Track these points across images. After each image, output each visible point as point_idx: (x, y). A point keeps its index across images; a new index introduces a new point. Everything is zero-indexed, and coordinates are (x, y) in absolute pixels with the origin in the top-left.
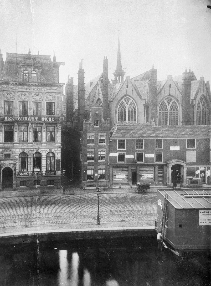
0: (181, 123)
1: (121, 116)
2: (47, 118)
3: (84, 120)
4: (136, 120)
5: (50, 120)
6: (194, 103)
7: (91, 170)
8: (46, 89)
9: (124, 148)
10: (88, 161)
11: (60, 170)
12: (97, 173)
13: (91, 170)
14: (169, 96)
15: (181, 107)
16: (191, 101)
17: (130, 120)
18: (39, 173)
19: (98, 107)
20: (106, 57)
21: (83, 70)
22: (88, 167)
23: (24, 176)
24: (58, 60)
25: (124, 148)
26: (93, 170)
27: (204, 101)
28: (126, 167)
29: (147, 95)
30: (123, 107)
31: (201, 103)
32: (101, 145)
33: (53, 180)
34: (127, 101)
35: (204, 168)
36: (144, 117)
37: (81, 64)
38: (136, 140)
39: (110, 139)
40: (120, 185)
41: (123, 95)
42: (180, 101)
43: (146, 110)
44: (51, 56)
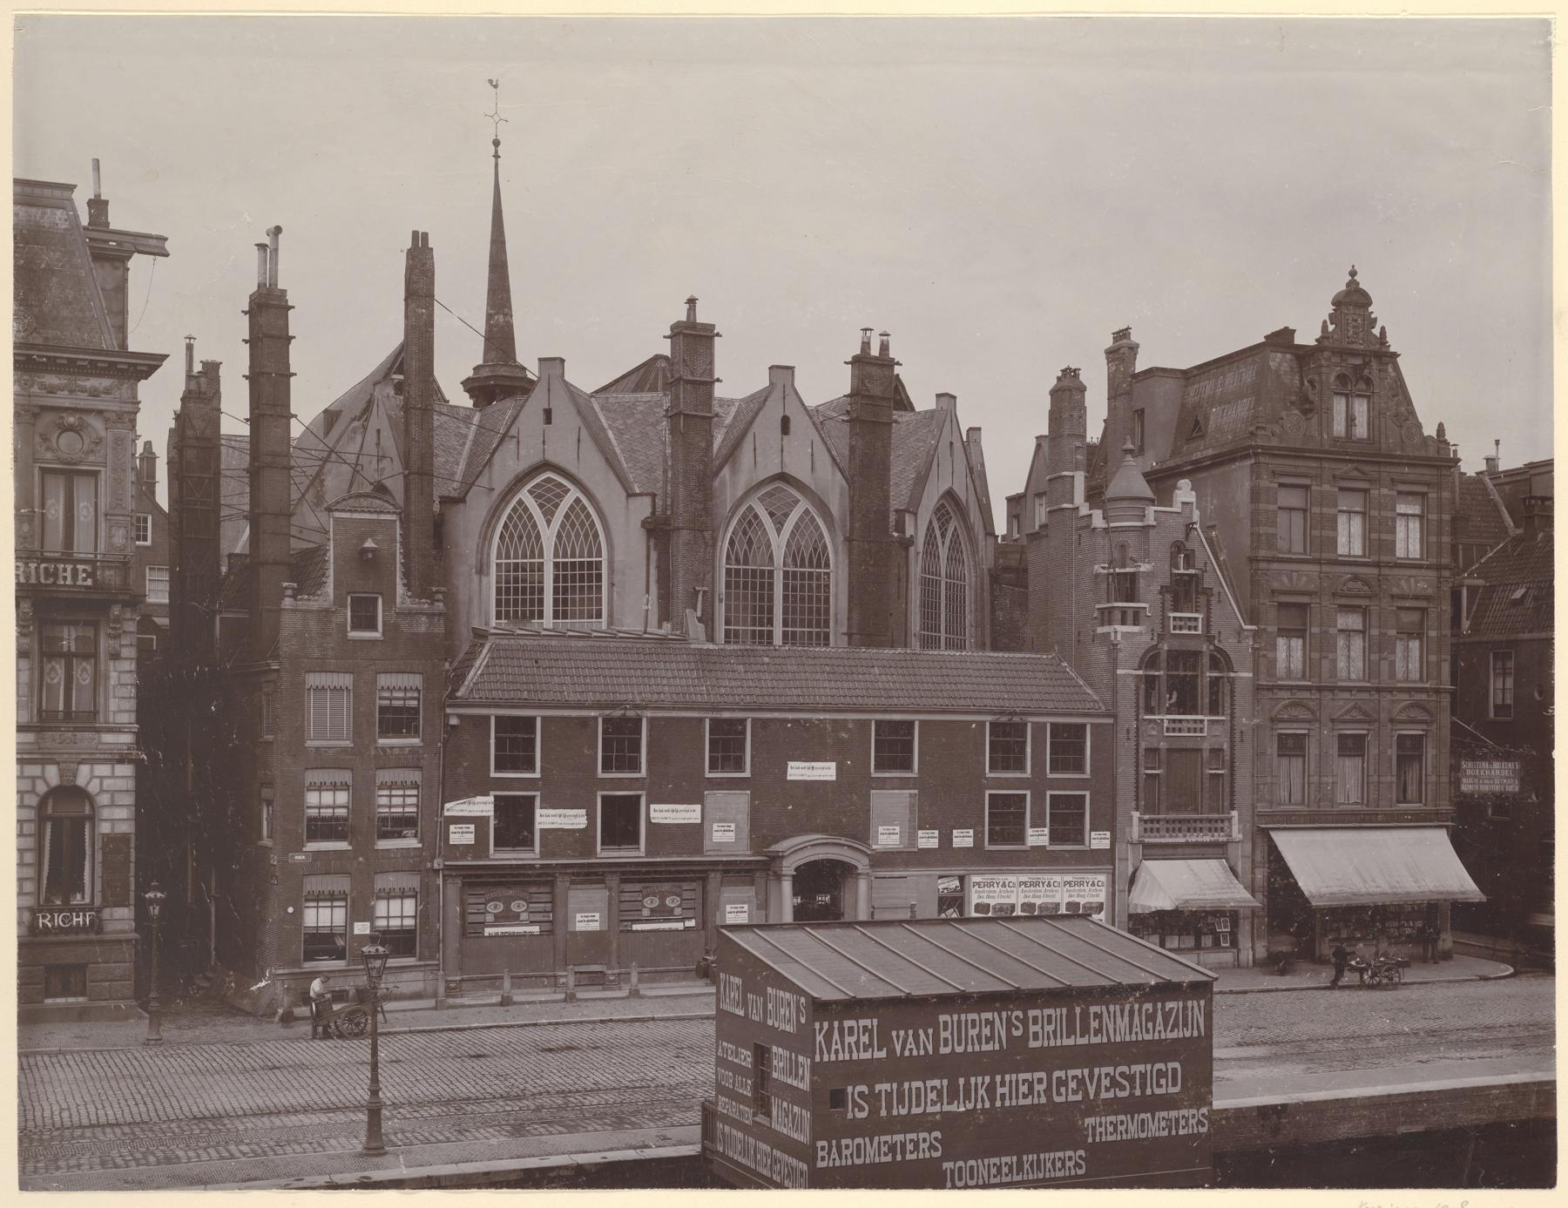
0: (846, 638)
1: (516, 602)
2: (43, 566)
3: (289, 592)
4: (599, 615)
5: (65, 578)
6: (909, 532)
7: (402, 896)
8: (43, 386)
9: (532, 768)
10: (312, 846)
11: (132, 902)
12: (369, 916)
13: (399, 901)
14: (778, 484)
15: (840, 548)
16: (893, 517)
17: (565, 617)
18: (78, 916)
19: (374, 516)
20: (425, 236)
21: (284, 292)
22: (313, 884)
23: (63, 938)
24: (119, 220)
25: (532, 768)
26: (413, 901)
27: (955, 529)
28: (545, 883)
29: (660, 472)
30: (522, 533)
31: (943, 536)
32: (392, 748)
33: (82, 968)
34: (549, 500)
35: (957, 883)
36: (648, 592)
37: (268, 251)
38: (600, 720)
39: (448, 711)
40: (507, 984)
41: (523, 465)
42: (835, 509)
43: (654, 556)
44: (76, 186)
